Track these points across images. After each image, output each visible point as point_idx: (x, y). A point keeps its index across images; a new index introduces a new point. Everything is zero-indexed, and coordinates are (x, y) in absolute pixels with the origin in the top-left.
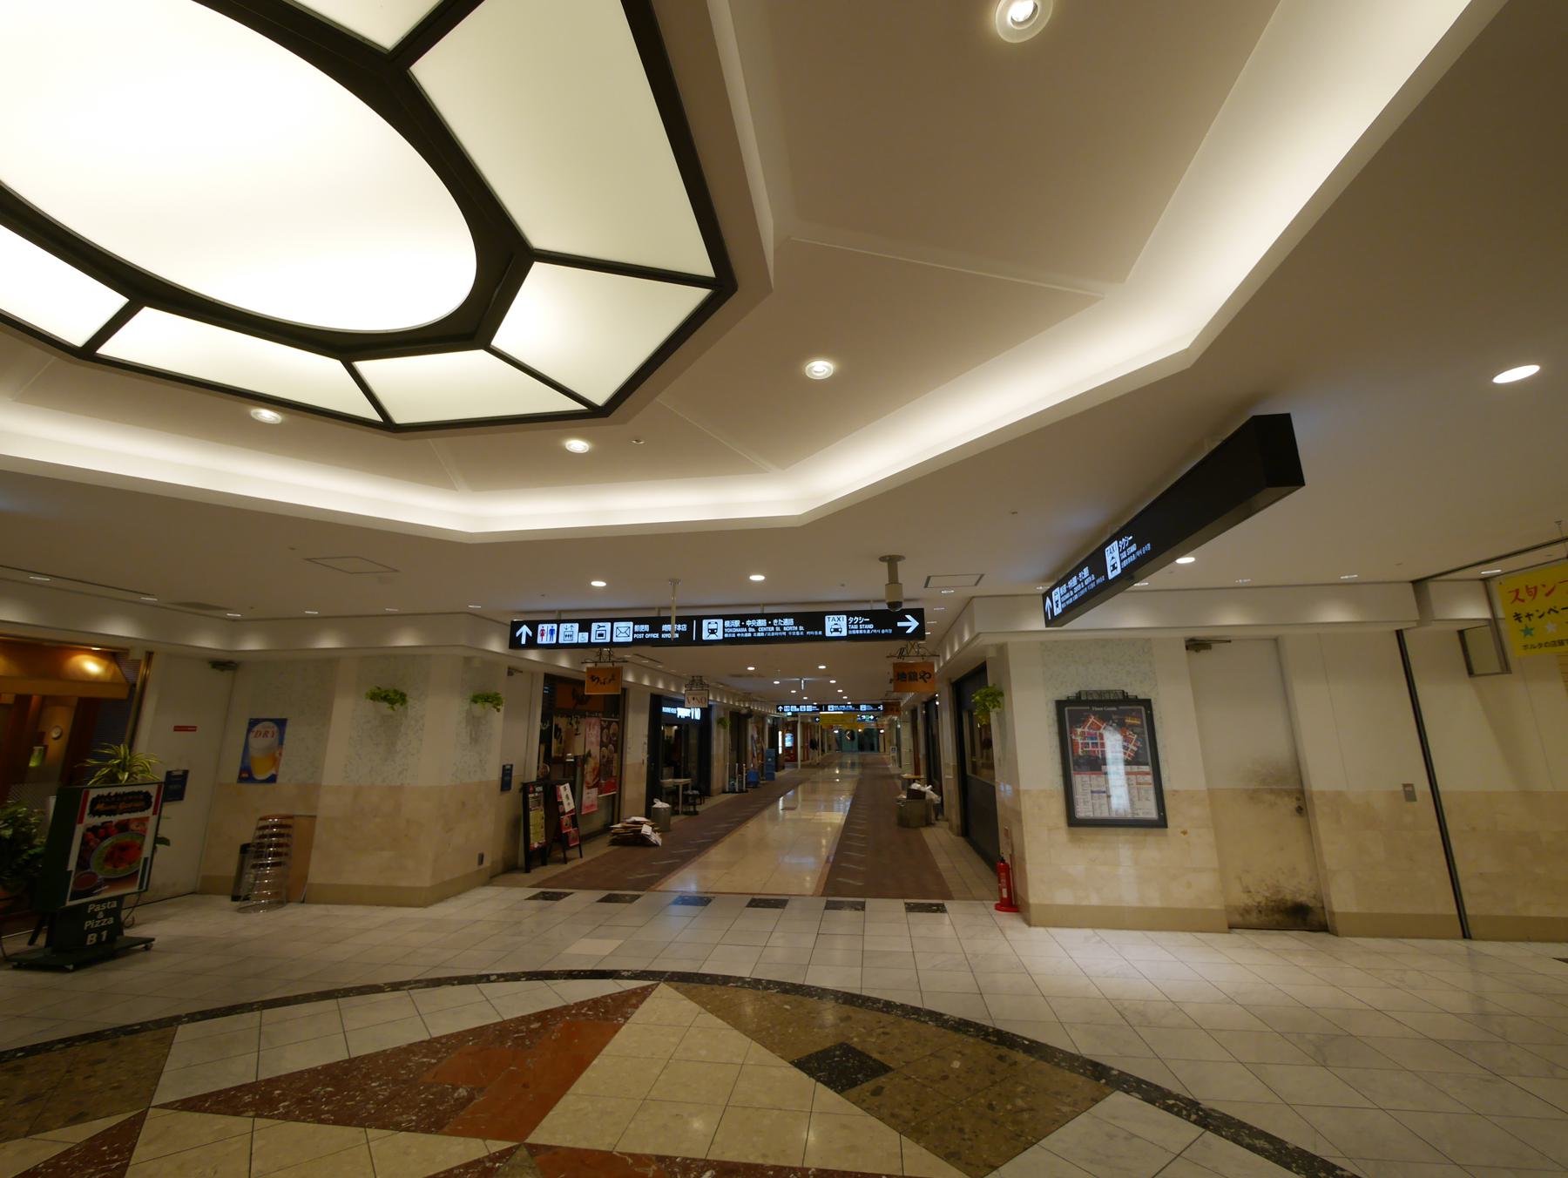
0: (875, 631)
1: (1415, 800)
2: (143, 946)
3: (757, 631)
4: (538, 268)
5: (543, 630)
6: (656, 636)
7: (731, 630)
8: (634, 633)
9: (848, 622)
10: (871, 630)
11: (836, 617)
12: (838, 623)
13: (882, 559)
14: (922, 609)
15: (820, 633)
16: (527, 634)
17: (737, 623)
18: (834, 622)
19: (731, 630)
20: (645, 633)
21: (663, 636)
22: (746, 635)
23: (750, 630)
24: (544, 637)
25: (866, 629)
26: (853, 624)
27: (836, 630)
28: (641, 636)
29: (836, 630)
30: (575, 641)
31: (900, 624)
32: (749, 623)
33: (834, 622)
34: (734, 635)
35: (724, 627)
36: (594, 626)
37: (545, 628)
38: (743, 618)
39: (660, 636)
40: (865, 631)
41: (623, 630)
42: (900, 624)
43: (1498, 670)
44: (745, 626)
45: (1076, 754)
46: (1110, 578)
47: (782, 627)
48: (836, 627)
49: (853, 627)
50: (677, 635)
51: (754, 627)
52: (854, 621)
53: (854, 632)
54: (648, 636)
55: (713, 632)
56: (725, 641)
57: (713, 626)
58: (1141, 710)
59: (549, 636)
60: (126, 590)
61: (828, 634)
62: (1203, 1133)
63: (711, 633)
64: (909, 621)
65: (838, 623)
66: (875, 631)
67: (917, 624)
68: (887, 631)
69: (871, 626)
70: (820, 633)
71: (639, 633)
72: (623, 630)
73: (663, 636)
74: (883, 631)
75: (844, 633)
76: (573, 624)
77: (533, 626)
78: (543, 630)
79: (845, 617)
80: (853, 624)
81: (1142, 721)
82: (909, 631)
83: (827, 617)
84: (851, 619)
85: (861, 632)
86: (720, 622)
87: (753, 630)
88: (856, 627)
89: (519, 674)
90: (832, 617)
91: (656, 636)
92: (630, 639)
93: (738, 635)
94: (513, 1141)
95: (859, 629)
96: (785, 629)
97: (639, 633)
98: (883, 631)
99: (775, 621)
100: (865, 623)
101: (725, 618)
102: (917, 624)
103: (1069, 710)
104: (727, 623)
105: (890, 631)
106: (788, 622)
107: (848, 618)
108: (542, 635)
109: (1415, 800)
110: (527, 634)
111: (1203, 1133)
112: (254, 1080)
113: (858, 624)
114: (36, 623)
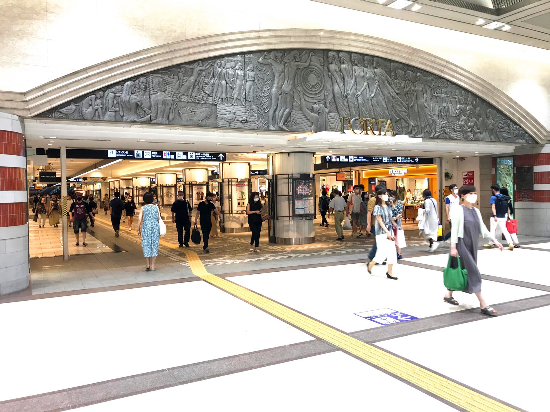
5: (165, 154)
7: (197, 156)
8: (152, 155)
13: (368, 134)
14: (314, 170)
16: (222, 156)
20: (156, 155)
22: (202, 158)
23: (204, 157)
24: (166, 156)
27: (385, 160)
28: (155, 156)
29: (385, 160)
30: (182, 158)
31: (328, 161)
32: (203, 154)
41: (148, 154)
42: (328, 161)
44: (202, 155)
45: (495, 135)
54: (157, 156)
55: (192, 157)
56: (402, 163)
57: (192, 155)
59: (167, 155)
60: (448, 19)
61: (135, 157)
69: (392, 160)
71: (154, 155)
72: (148, 154)
78: (165, 154)
82: (223, 156)
86: (400, 157)
87: (205, 157)
89: (288, 155)
92: (150, 157)
97: (154, 155)
104: (196, 154)
106: (207, 155)
108: (165, 155)
110: (222, 156)
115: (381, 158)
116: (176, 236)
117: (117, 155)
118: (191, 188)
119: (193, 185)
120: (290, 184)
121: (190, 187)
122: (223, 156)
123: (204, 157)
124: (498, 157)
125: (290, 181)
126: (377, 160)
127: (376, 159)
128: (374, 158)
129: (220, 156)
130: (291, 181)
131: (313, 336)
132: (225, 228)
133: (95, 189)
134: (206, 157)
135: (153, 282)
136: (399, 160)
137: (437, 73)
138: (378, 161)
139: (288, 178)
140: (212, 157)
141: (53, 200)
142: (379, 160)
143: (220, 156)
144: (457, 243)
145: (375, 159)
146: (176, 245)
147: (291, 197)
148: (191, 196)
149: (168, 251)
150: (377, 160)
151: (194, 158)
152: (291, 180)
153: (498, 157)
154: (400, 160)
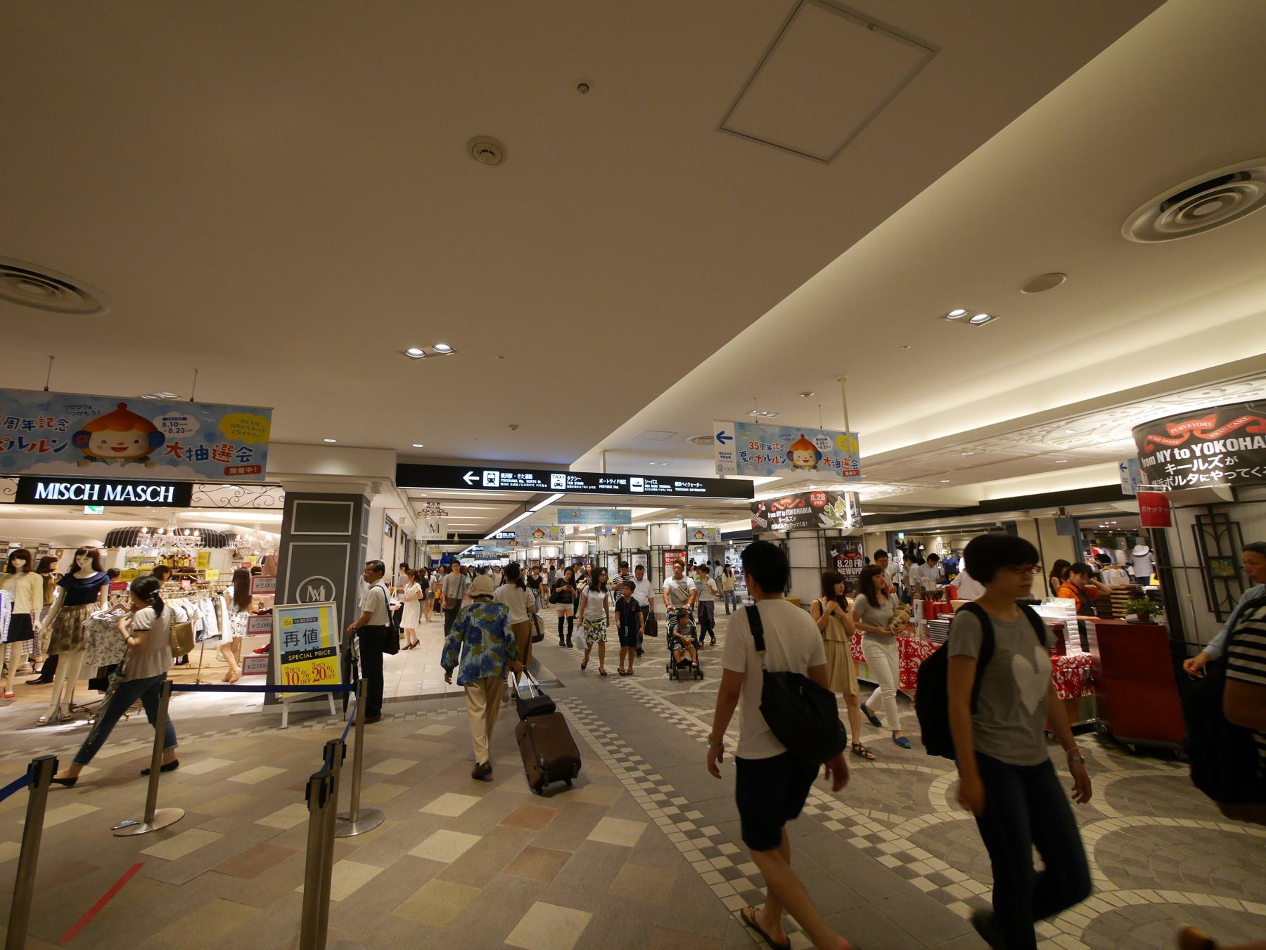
0: (585, 487)
1: (655, 635)
3: (525, 482)
4: (14, 501)
7: (505, 480)
9: (567, 479)
11: (558, 475)
12: (560, 479)
15: (546, 486)
17: (510, 475)
19: (505, 480)
23: (521, 481)
26: (570, 481)
27: (558, 485)
29: (558, 485)
34: (508, 485)
36: (485, 473)
38: (515, 472)
40: (578, 487)
43: (14, 501)
44: (516, 478)
48: (558, 482)
50: (617, 487)
51: (522, 479)
53: (570, 487)
55: (491, 480)
57: (492, 477)
58: (298, 504)
62: (948, 869)
63: (490, 482)
64: (470, 480)
65: (560, 479)
66: (585, 487)
67: (464, 478)
69: (582, 483)
73: (600, 486)
75: (564, 487)
76: (562, 475)
79: (565, 476)
80: (570, 481)
82: (471, 473)
83: (552, 475)
84: (569, 478)
85: (575, 487)
86: (497, 473)
87: (522, 481)
88: (572, 483)
90: (556, 475)
93: (511, 484)
95: (574, 485)
96: (527, 481)
98: (590, 488)
99: (519, 475)
100: (578, 481)
101: (501, 471)
102: (464, 478)
103: (298, 504)
104: (503, 475)
106: (529, 476)
107: (567, 477)
109: (655, 635)
111: (948, 869)
114: (275, 472)
115: (623, 482)
117: (568, 487)
118: (661, 556)
119: (665, 551)
120: (821, 548)
121: (659, 554)
123: (521, 481)
124: (231, 467)
125: (820, 543)
126: (613, 484)
127: (609, 484)
128: (601, 481)
129: (470, 480)
130: (824, 543)
131: (1240, 903)
133: (543, 556)
134: (525, 482)
135: (575, 744)
139: (818, 538)
141: (1089, 601)
142: (619, 485)
143: (470, 480)
145: (604, 484)
146: (31, 641)
147: (661, 570)
148: (661, 570)
149: (639, 683)
150: (613, 484)
151: (497, 485)
152: (824, 540)
153: (231, 467)
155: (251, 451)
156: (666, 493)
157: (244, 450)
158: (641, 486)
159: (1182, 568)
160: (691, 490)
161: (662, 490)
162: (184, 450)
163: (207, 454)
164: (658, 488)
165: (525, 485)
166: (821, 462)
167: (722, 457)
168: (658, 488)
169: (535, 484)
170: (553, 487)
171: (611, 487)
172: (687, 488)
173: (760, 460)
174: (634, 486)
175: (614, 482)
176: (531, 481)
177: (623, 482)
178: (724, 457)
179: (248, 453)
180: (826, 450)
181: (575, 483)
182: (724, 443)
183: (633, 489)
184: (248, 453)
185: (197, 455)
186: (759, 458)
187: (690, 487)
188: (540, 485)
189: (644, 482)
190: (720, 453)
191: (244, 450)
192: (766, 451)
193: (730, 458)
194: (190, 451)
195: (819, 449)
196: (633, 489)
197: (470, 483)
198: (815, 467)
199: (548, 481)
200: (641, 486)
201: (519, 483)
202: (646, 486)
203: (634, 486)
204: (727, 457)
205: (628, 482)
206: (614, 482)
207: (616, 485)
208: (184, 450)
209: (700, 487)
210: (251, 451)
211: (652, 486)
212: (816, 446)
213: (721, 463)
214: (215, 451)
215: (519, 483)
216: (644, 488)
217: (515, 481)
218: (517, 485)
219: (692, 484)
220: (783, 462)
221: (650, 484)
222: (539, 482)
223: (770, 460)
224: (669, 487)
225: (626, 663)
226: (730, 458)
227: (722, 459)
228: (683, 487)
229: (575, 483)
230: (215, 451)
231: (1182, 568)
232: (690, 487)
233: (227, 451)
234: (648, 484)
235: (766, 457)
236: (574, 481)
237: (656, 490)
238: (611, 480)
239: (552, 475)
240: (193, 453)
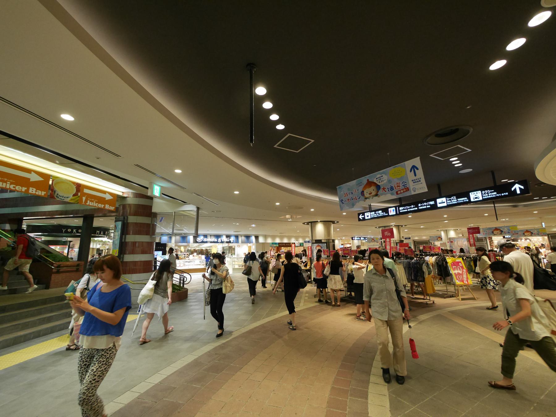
0: (498, 195)
2: (276, 292)
3: (379, 215)
5: (390, 210)
6: (416, 209)
9: (482, 194)
10: (495, 195)
11: (475, 192)
12: (477, 195)
15: (387, 214)
16: (520, 188)
17: (373, 213)
18: (475, 195)
21: (419, 208)
25: (493, 195)
33: (475, 195)
34: (373, 217)
35: (370, 215)
36: (366, 214)
37: (391, 209)
39: (418, 208)
40: (492, 196)
44: (376, 213)
46: (31, 181)
47: (379, 214)
48: (476, 197)
49: (485, 195)
50: (429, 206)
52: (485, 193)
53: (486, 197)
55: (368, 216)
56: (371, 218)
65: (477, 195)
66: (498, 195)
68: (505, 194)
69: (495, 193)
70: (387, 214)
73: (419, 208)
74: (503, 194)
75: (481, 199)
76: (478, 192)
77: (363, 214)
78: (390, 210)
79: (480, 192)
81: (182, 246)
82: (361, 215)
83: (470, 193)
84: (483, 192)
85: (490, 197)
86: (369, 213)
87: (378, 214)
90: (473, 193)
91: (416, 209)
94: (135, 191)
95: (488, 195)
96: (380, 214)
98: (503, 194)
99: (377, 212)
100: (491, 192)
104: (371, 213)
105: (507, 194)
106: (380, 212)
107: (482, 192)
108: (391, 212)
110: (520, 188)
112: (370, 382)
113: (488, 193)
116: (203, 295)
122: (522, 187)
123: (378, 214)
126: (426, 205)
127: (424, 206)
132: (128, 223)
136: (368, 216)
137: (28, 332)
138: (428, 207)
140: (384, 213)
142: (430, 205)
143: (515, 189)
144: (161, 243)
145: (422, 206)
150: (426, 205)
151: (370, 218)
154: (370, 216)
155: (406, 182)
156: (464, 203)
157: (404, 183)
158: (444, 202)
159: (312, 239)
160: (409, 210)
161: (460, 202)
162: (387, 189)
163: (393, 188)
164: (457, 201)
165: (379, 216)
166: (381, 191)
167: (414, 183)
168: (457, 201)
169: (383, 214)
170: (472, 200)
171: (425, 207)
172: (406, 209)
173: (349, 201)
174: (440, 203)
175: (427, 204)
176: (381, 214)
177: (432, 203)
178: (416, 182)
179: (405, 183)
180: (382, 183)
181: (489, 194)
182: (411, 171)
183: (439, 205)
184: (405, 183)
185: (391, 189)
186: (348, 200)
187: (408, 209)
188: (385, 215)
189: (446, 200)
190: (413, 181)
191: (404, 183)
192: (351, 196)
193: (420, 181)
194: (388, 189)
195: (378, 184)
196: (439, 205)
197: (362, 219)
198: (377, 195)
199: (469, 198)
200: (444, 202)
201: (377, 215)
202: (448, 202)
203: (440, 203)
204: (418, 182)
205: (436, 202)
206: (405, 208)
207: (428, 205)
208: (387, 189)
209: (414, 208)
210: (406, 182)
211: (452, 201)
212: (377, 182)
213: (414, 187)
214: (395, 186)
215: (377, 215)
216: (447, 203)
217: (376, 215)
218: (376, 216)
219: (409, 207)
220: (359, 199)
221: (451, 200)
222: (384, 213)
223: (353, 199)
224: (466, 198)
225: (409, 251)
226: (420, 181)
227: (415, 184)
228: (404, 209)
229: (489, 194)
230: (395, 186)
231: (312, 239)
232: (408, 209)
233: (398, 185)
234: (449, 200)
235: (355, 198)
236: (488, 193)
237: (456, 202)
238: (425, 204)
239: (470, 193)
240: (389, 189)
